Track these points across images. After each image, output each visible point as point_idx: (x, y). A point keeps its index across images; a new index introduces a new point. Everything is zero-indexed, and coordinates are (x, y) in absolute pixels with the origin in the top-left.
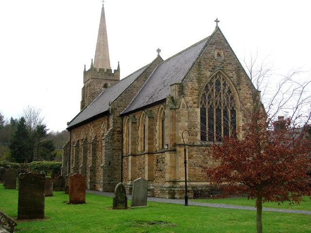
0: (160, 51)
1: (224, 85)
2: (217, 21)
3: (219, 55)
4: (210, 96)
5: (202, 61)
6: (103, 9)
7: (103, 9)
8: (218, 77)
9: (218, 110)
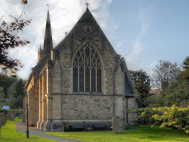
2: (87, 4)
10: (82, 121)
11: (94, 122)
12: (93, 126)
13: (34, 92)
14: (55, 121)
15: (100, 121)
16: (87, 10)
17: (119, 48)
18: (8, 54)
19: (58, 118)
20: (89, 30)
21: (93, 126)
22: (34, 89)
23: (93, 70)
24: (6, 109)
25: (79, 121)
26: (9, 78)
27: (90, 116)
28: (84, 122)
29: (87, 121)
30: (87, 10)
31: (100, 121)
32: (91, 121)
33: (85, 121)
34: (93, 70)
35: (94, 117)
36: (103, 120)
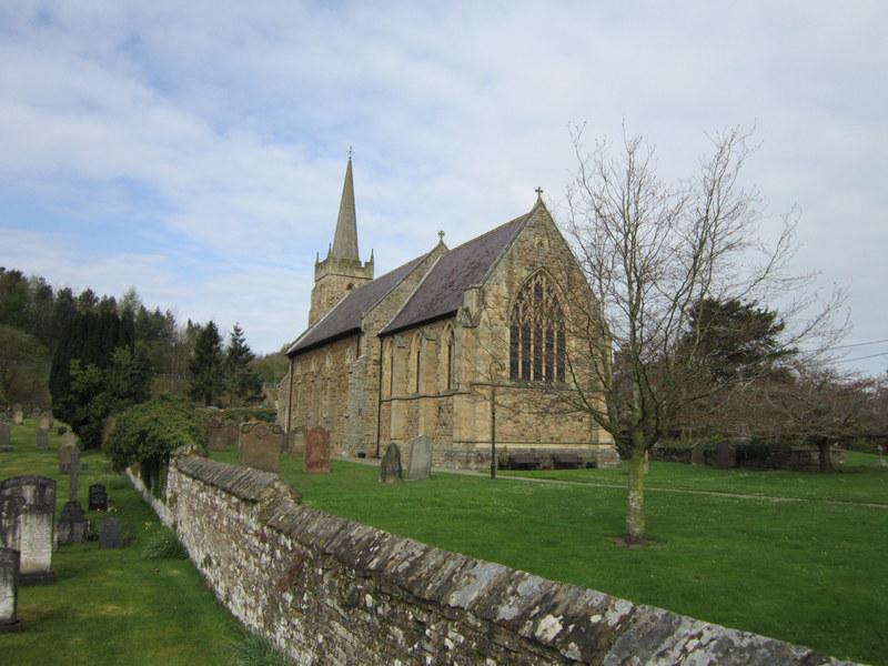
1: (549, 291)
2: (539, 191)
3: (541, 244)
4: (525, 309)
5: (515, 253)
6: (350, 162)
7: (350, 162)
8: (539, 278)
9: (538, 333)
10: (528, 446)
11: (554, 450)
12: (554, 458)
13: (367, 371)
14: (478, 446)
15: (563, 447)
16: (541, 203)
17: (187, 309)
18: (211, 322)
19: (485, 440)
20: (542, 245)
21: (554, 458)
22: (366, 365)
23: (549, 334)
24: (101, 294)
25: (522, 446)
26: (163, 317)
27: (544, 437)
28: (533, 450)
29: (537, 447)
30: (541, 203)
31: (563, 447)
32: (545, 446)
33: (533, 446)
34: (549, 334)
35: (552, 439)
36: (570, 447)
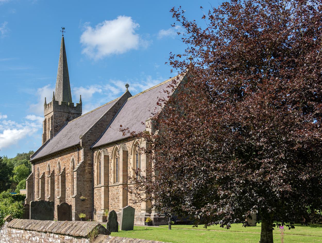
0: (129, 86)
